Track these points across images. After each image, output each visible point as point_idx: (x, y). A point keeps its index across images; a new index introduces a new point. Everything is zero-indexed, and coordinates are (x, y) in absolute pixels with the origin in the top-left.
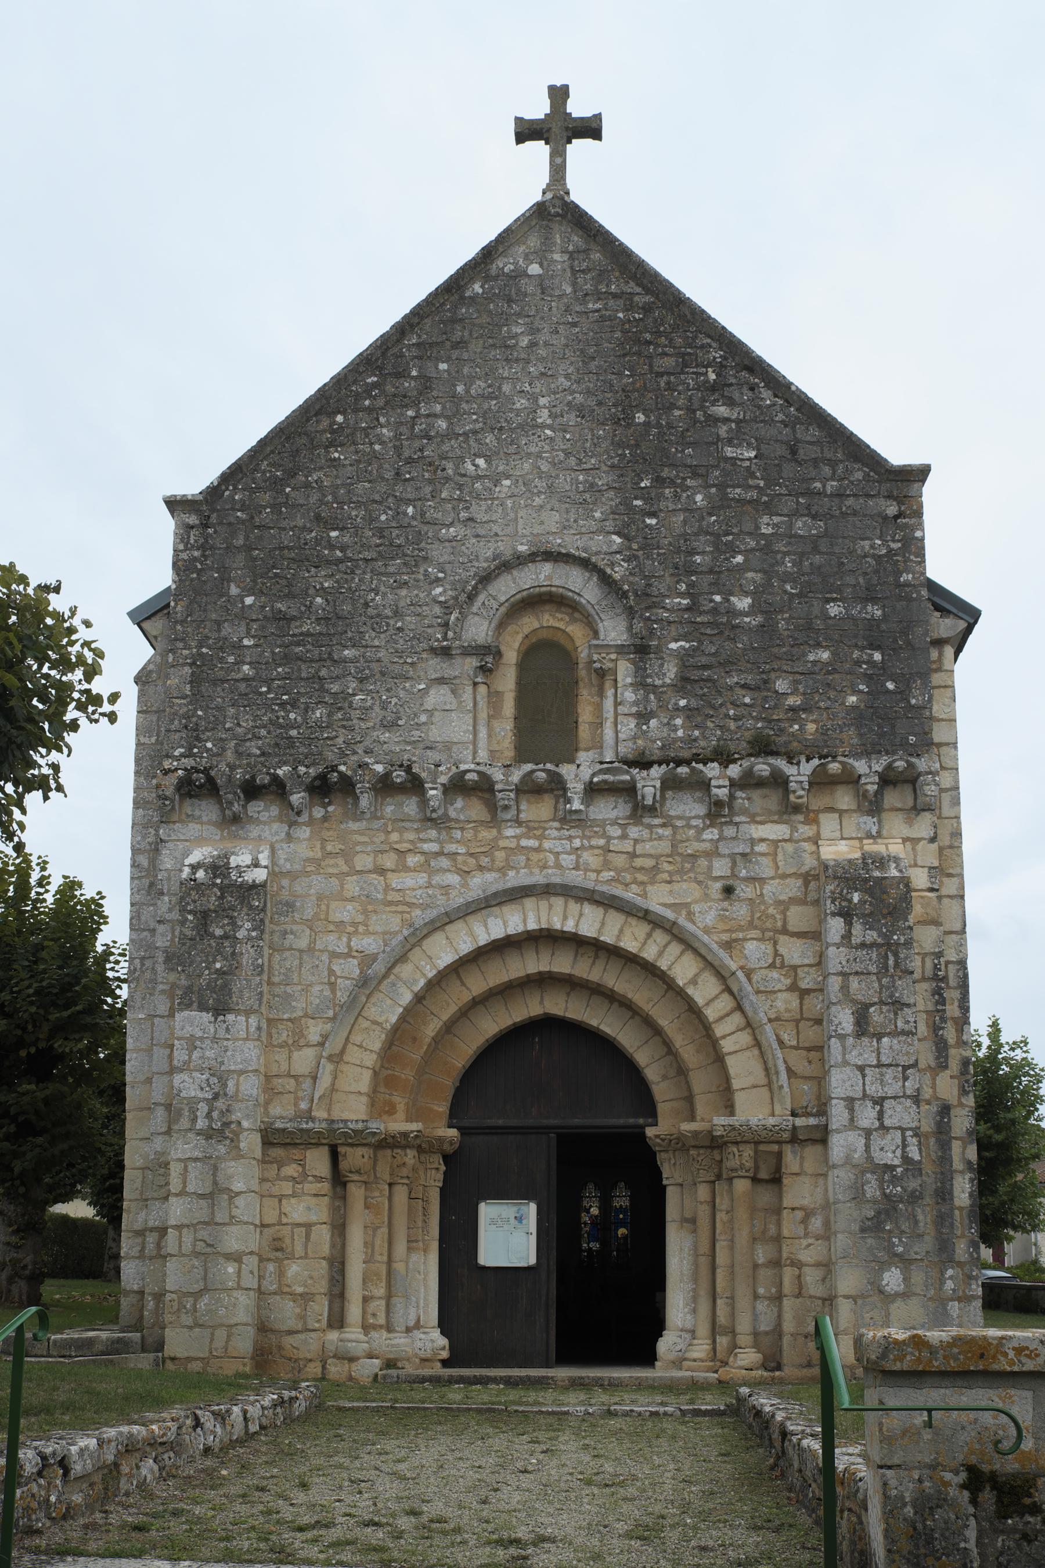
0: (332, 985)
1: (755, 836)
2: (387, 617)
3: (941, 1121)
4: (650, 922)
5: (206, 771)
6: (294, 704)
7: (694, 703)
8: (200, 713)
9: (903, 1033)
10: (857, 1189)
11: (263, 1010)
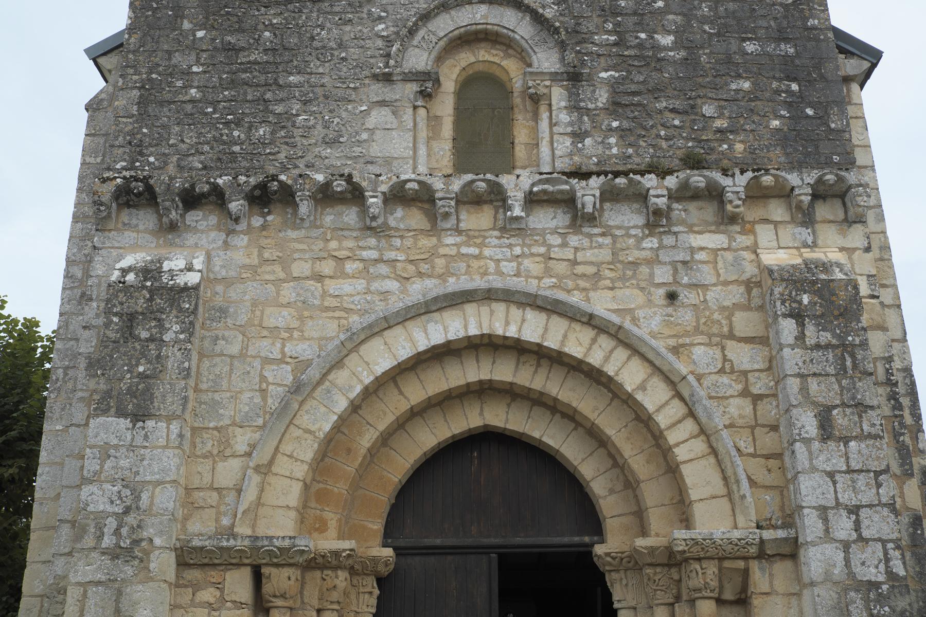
0: (263, 391)
1: (694, 245)
2: (332, 49)
3: (915, 533)
4: (594, 327)
5: (145, 180)
6: (238, 123)
7: (626, 124)
8: (145, 130)
9: (870, 436)
10: (841, 609)
11: (187, 416)
